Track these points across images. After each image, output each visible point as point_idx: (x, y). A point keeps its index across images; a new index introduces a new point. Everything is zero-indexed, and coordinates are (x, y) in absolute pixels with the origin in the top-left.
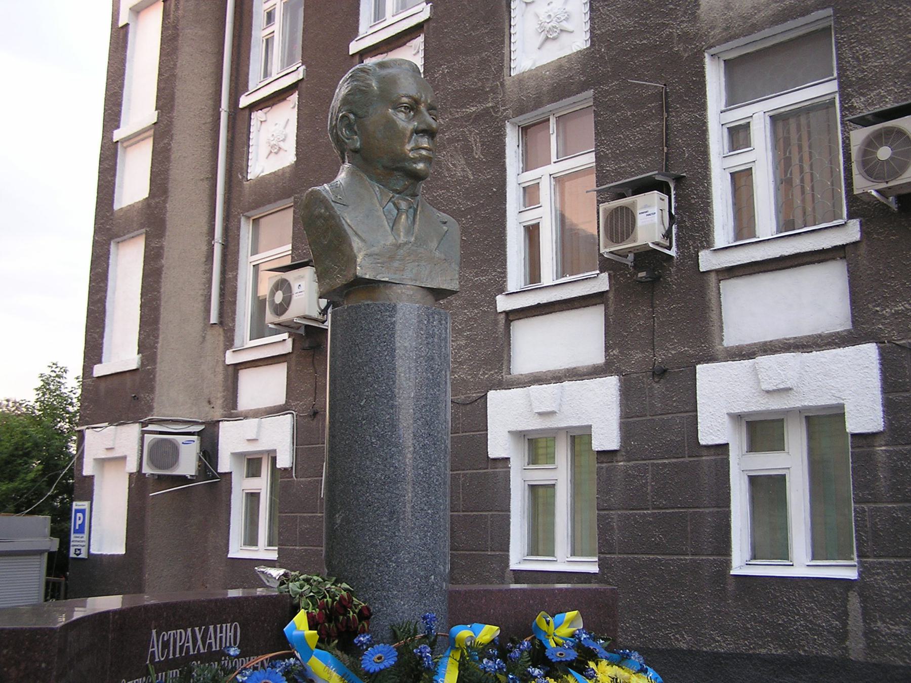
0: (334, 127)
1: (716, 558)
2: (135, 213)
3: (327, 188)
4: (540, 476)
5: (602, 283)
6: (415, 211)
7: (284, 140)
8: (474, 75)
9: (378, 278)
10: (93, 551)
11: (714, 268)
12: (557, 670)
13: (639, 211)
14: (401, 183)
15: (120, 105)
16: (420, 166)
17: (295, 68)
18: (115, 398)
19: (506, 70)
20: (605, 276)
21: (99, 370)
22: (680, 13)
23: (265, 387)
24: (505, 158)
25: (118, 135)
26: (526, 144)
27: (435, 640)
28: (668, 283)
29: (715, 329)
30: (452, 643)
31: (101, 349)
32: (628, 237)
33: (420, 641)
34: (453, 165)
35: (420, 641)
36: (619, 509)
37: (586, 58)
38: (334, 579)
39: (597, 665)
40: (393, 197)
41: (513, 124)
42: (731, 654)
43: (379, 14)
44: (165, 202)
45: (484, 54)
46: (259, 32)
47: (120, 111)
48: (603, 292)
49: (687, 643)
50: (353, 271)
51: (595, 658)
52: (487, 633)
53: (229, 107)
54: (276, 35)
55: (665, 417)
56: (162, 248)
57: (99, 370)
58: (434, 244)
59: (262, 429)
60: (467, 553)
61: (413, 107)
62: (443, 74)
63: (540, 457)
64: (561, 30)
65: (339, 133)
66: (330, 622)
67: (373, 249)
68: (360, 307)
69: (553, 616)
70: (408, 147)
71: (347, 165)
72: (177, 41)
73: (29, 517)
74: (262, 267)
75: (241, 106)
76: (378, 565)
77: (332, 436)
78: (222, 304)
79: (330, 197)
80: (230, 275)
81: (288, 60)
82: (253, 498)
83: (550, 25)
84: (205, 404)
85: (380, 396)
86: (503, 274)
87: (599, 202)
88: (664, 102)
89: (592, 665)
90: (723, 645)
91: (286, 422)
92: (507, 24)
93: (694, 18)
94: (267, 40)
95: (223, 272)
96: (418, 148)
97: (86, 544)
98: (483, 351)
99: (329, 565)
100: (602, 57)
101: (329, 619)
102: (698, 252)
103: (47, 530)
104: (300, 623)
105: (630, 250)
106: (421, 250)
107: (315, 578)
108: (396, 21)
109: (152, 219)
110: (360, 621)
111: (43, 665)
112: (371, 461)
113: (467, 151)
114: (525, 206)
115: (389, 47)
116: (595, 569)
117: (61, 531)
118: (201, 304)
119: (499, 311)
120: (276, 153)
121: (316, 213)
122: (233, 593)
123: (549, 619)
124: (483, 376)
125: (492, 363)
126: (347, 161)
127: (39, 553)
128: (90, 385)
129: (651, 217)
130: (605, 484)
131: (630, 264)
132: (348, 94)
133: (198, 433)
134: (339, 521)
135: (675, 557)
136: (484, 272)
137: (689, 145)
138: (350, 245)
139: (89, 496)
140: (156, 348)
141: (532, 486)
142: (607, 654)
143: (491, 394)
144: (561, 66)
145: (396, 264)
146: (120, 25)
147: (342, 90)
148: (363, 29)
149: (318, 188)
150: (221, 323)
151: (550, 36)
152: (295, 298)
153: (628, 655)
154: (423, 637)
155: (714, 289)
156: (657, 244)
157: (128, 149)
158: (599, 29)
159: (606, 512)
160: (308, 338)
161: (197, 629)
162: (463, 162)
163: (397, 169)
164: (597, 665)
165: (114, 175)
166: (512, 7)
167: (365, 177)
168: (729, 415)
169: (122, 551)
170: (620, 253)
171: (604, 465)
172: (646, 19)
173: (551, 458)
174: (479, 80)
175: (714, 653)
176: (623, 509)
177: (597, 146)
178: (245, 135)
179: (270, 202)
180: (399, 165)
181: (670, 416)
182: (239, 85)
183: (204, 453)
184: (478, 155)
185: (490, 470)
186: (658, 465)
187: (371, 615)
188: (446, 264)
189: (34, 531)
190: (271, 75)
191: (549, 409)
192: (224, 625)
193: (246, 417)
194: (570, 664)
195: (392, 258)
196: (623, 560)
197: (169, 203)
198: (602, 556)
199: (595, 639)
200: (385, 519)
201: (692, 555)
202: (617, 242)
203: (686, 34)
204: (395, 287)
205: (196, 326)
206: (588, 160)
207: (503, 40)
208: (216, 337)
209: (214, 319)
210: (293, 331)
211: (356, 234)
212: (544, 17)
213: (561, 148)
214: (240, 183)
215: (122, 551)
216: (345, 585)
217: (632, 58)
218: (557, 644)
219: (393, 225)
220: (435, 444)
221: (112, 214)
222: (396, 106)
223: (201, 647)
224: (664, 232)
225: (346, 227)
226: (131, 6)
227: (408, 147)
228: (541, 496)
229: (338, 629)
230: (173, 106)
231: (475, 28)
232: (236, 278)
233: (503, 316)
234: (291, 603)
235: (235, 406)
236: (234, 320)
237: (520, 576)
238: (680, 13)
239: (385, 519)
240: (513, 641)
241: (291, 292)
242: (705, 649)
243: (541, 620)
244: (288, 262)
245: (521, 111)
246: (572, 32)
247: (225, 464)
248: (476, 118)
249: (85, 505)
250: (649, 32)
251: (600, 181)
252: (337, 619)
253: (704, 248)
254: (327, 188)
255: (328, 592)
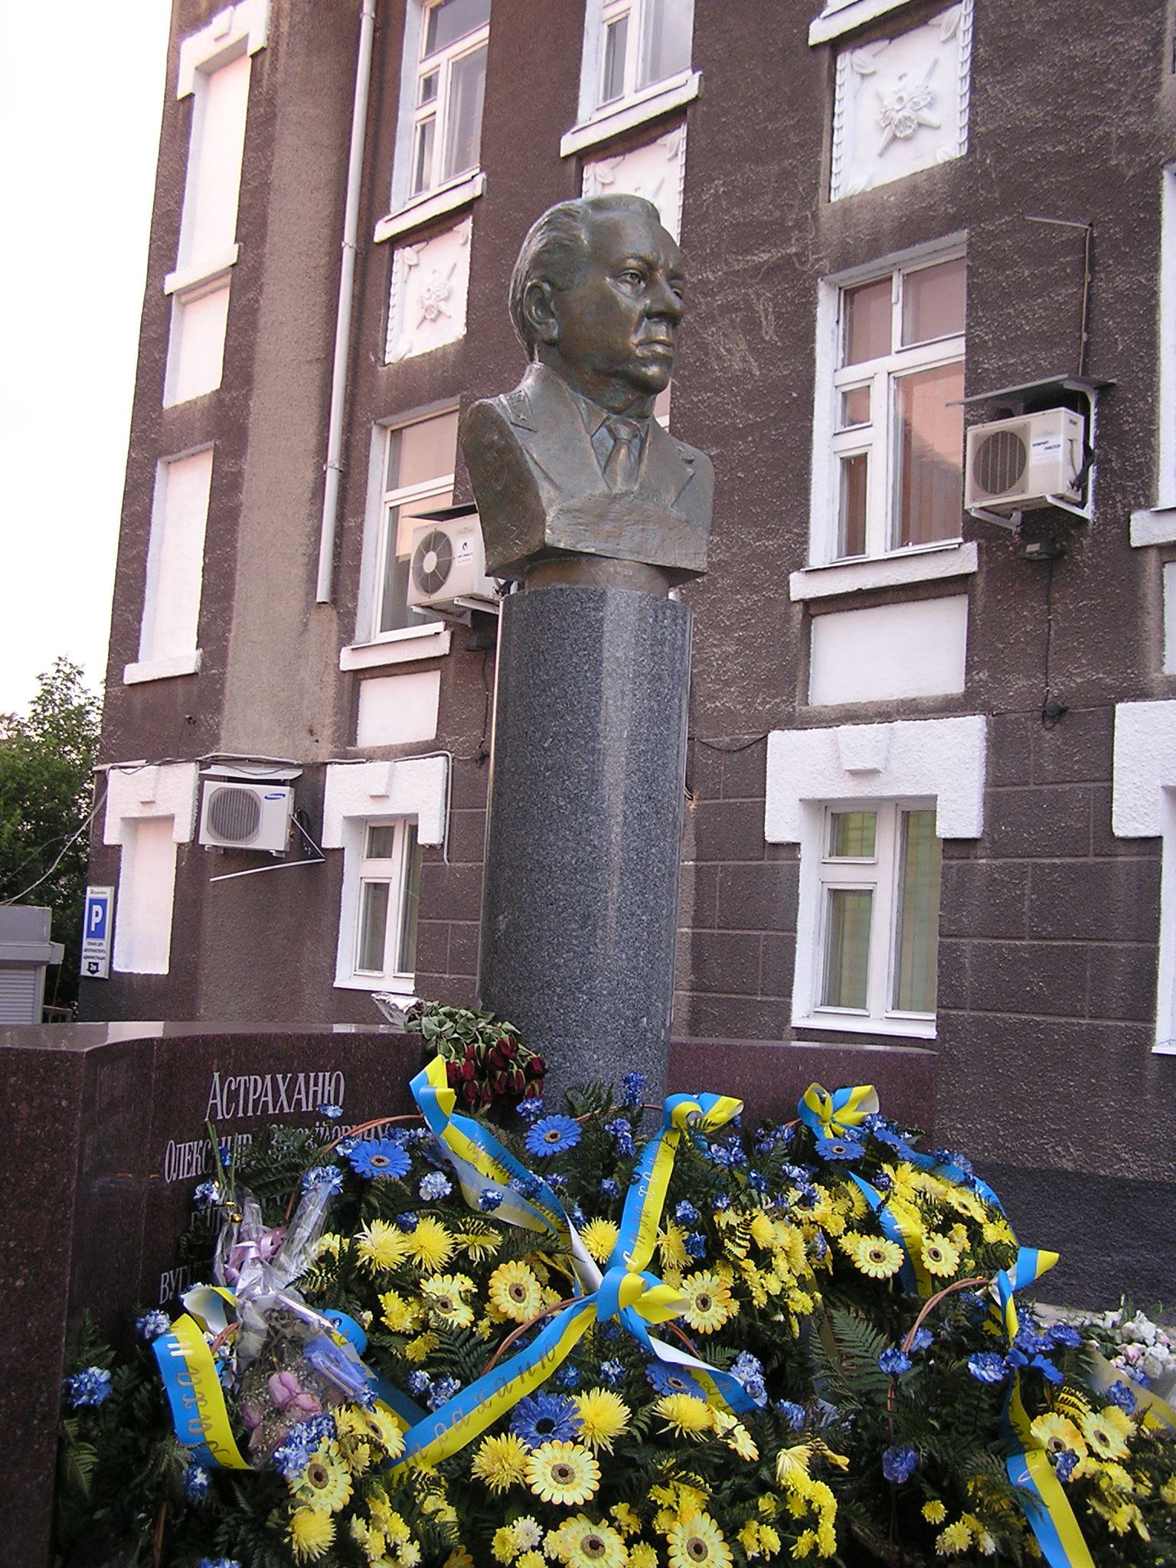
0: (518, 303)
1: (1129, 1024)
2: (198, 415)
3: (505, 402)
4: (848, 875)
5: (966, 560)
6: (643, 441)
7: (447, 299)
8: (768, 198)
9: (579, 548)
10: (116, 968)
11: (1154, 542)
12: (832, 1174)
13: (1032, 442)
14: (622, 396)
15: (176, 232)
16: (653, 370)
17: (468, 177)
18: (161, 720)
19: (821, 192)
20: (972, 547)
21: (133, 674)
22: (1125, 99)
23: (402, 710)
24: (814, 341)
25: (172, 283)
26: (851, 321)
27: (640, 1114)
28: (1076, 564)
29: (1151, 645)
30: (667, 1121)
31: (138, 638)
32: (1012, 483)
33: (616, 1114)
34: (728, 350)
35: (616, 1114)
36: (974, 936)
37: (959, 173)
38: (492, 1015)
39: (895, 1169)
40: (608, 418)
41: (830, 284)
42: (1146, 1182)
43: (612, 86)
44: (247, 397)
45: (786, 163)
46: (410, 113)
47: (177, 243)
48: (967, 575)
49: (1074, 1161)
50: (538, 536)
51: (894, 1159)
52: (723, 1108)
53: (357, 241)
54: (439, 118)
55: (1060, 788)
56: (240, 473)
57: (133, 674)
58: (671, 497)
59: (396, 780)
60: (724, 996)
61: (645, 274)
62: (716, 195)
63: (851, 845)
64: (920, 125)
65: (526, 313)
66: (481, 1078)
67: (571, 502)
68: (548, 592)
69: (832, 1092)
70: (635, 339)
71: (537, 365)
72: (272, 125)
73: (17, 908)
74: (405, 511)
75: (377, 239)
76: (560, 997)
77: (498, 794)
78: (336, 570)
79: (508, 416)
80: (351, 523)
81: (458, 163)
82: (377, 891)
83: (901, 114)
84: (304, 733)
85: (575, 735)
86: (803, 538)
87: (968, 423)
88: (1088, 256)
89: (887, 1168)
90: (1132, 1168)
91: (434, 771)
92: (828, 112)
93: (1150, 106)
94: (423, 127)
95: (340, 517)
96: (649, 342)
97: (107, 955)
98: (764, 665)
99: (485, 994)
100: (986, 173)
101: (481, 1074)
102: (1129, 513)
103: (47, 930)
104: (434, 1079)
105: (1015, 506)
106: (650, 506)
107: (463, 1012)
108: (643, 99)
109: (225, 425)
110: (529, 1079)
111: (64, 1103)
112: (557, 834)
113: (751, 327)
114: (844, 424)
115: (628, 145)
116: (930, 1032)
117: (69, 931)
118: (302, 569)
119: (793, 599)
120: (434, 320)
121: (485, 441)
122: (339, 1028)
123: (826, 1095)
124: (762, 706)
125: (781, 686)
126: (537, 357)
127: (35, 965)
128: (117, 698)
129: (1053, 453)
130: (954, 894)
131: (1014, 529)
132: (540, 252)
133: (292, 783)
134: (503, 927)
135: (1063, 1020)
136: (772, 533)
137: (1124, 331)
138: (538, 498)
139: (112, 879)
140: (227, 640)
141: (836, 891)
142: (914, 1155)
143: (775, 737)
144: (915, 187)
145: (608, 527)
146: (180, 95)
147: (533, 244)
148: (586, 110)
149: (490, 401)
150: (334, 601)
151: (900, 132)
152: (457, 564)
153: (946, 1158)
154: (620, 1109)
155: (1153, 577)
156: (1061, 498)
157: (190, 307)
158: (985, 124)
159: (953, 940)
160: (473, 628)
161: (279, 1077)
162: (744, 346)
163: (616, 375)
164: (895, 1169)
165: (165, 351)
166: (838, 81)
167: (565, 386)
168: (1166, 788)
169: (164, 969)
170: (998, 510)
171: (954, 862)
172: (1066, 107)
173: (867, 847)
174: (777, 207)
175: (1117, 1180)
176: (982, 936)
177: (969, 327)
178: (383, 288)
179: (420, 403)
180: (619, 368)
181: (1067, 787)
182: (375, 203)
183: (300, 815)
184: (769, 334)
185: (766, 863)
186: (1042, 867)
187: (546, 1071)
188: (688, 529)
189: (22, 930)
190: (428, 188)
191: (869, 766)
192: (321, 1075)
193: (370, 759)
194: (854, 1166)
195: (602, 517)
196: (978, 1021)
197: (254, 398)
198: (943, 1011)
199: (898, 1132)
200: (574, 926)
201: (1091, 1017)
202: (994, 492)
203: (1134, 135)
204: (605, 563)
205: (291, 606)
206: (954, 349)
207: (820, 140)
208: (326, 623)
209: (322, 595)
210: (452, 619)
211: (547, 477)
212: (890, 102)
213: (909, 327)
214: (372, 368)
215: (164, 969)
216: (508, 1026)
217: (1037, 176)
218: (835, 1135)
219: (607, 463)
220: (657, 813)
221: (161, 416)
222: (618, 273)
223: (285, 1103)
224: (1073, 478)
225: (531, 464)
226: (197, 63)
227: (635, 339)
228: (847, 908)
229: (493, 1090)
230: (263, 237)
231: (772, 117)
232: (360, 528)
233: (799, 607)
234: (424, 1048)
235: (352, 739)
236: (355, 598)
237: (803, 1033)
238: (1125, 99)
239: (574, 926)
240: (766, 1126)
241: (451, 555)
242: (1102, 1173)
243: (812, 1096)
244: (447, 503)
245: (843, 262)
246: (938, 128)
247: (333, 836)
248: (771, 271)
249: (107, 892)
250: (1067, 132)
251: (971, 387)
252: (493, 1076)
253: (1140, 507)
254: (505, 402)
255: (481, 1033)
